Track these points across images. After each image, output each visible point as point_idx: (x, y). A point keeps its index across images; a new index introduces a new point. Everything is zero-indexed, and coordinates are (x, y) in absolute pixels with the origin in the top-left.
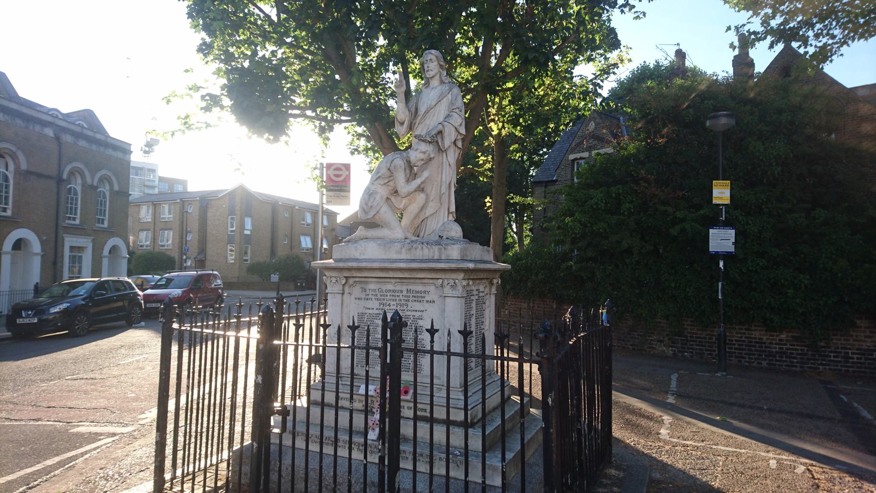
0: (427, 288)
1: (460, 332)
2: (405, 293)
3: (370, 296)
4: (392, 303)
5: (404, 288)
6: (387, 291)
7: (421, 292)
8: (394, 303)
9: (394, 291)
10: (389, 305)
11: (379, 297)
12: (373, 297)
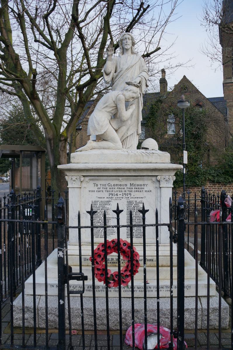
0: (146, 182)
2: (129, 186)
3: (101, 189)
4: (119, 193)
5: (128, 183)
6: (114, 185)
7: (141, 185)
8: (121, 193)
9: (121, 185)
10: (117, 195)
11: (108, 189)
12: (104, 190)
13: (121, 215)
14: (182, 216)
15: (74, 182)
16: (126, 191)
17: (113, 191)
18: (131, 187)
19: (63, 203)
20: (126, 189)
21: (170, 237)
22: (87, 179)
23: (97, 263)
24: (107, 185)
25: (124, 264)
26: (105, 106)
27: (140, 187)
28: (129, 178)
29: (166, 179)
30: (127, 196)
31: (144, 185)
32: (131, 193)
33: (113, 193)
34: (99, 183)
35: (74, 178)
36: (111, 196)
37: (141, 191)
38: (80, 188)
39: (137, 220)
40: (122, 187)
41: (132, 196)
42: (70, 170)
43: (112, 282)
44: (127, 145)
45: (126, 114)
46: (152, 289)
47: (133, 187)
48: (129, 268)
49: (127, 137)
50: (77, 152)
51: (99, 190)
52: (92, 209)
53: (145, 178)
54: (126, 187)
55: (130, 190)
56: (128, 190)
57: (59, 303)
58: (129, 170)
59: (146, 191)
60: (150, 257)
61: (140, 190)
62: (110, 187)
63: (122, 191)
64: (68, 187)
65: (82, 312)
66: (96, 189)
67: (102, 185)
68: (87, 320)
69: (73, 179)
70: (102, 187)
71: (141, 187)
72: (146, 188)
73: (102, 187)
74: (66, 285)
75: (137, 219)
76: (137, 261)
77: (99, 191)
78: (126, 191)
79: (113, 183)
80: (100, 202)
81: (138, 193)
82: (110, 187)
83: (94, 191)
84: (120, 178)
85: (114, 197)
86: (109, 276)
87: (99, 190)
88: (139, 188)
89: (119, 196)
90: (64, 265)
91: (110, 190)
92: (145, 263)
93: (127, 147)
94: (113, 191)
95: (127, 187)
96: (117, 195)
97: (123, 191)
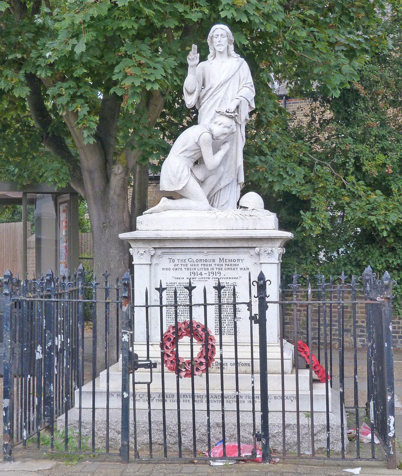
0: (241, 256)
1: (214, 287)
2: (217, 262)
3: (180, 266)
4: (204, 272)
5: (217, 257)
6: (197, 261)
7: (234, 261)
8: (207, 272)
9: (206, 261)
10: (201, 274)
11: (189, 267)
12: (183, 267)
13: (193, 291)
14: (262, 294)
15: (142, 257)
16: (213, 269)
17: (195, 269)
18: (221, 263)
19: (128, 279)
20: (213, 266)
21: (250, 318)
22: (159, 252)
23: (167, 348)
24: (187, 261)
25: (198, 348)
26: (183, 149)
27: (233, 263)
28: (217, 250)
29: (267, 252)
30: (214, 276)
31: (239, 260)
32: (220, 271)
33: (195, 271)
34: (177, 257)
35: (142, 251)
36: (193, 275)
37: (234, 269)
38: (150, 264)
39: (229, 310)
40: (208, 263)
41: (222, 276)
42: (136, 240)
43: (184, 370)
44: (220, 202)
45: (212, 160)
46: (244, 400)
47: (224, 264)
48: (204, 354)
49: (221, 189)
50: (145, 214)
51: (176, 267)
52: (161, 285)
53: (240, 250)
54: (213, 264)
55: (219, 267)
56: (216, 267)
57: (123, 396)
58: (217, 240)
59: (241, 269)
60: (245, 360)
61: (233, 267)
62: (192, 263)
63: (208, 269)
64: (133, 263)
65: (150, 426)
66: (172, 266)
67: (180, 261)
68: (157, 437)
69: (140, 253)
70: (180, 263)
71: (234, 263)
72: (241, 265)
73: (180, 263)
74: (131, 375)
75: (229, 308)
76: (213, 346)
77: (176, 269)
78: (213, 269)
79: (195, 257)
80: (178, 284)
81: (230, 271)
82: (192, 263)
83: (170, 269)
84: (205, 251)
85: (197, 277)
86: (181, 363)
87: (176, 267)
88: (231, 265)
89: (204, 276)
90: (129, 351)
91: (192, 267)
92: (221, 348)
93: (221, 204)
94: (195, 269)
95: (214, 263)
96: (202, 275)
97: (210, 269)
